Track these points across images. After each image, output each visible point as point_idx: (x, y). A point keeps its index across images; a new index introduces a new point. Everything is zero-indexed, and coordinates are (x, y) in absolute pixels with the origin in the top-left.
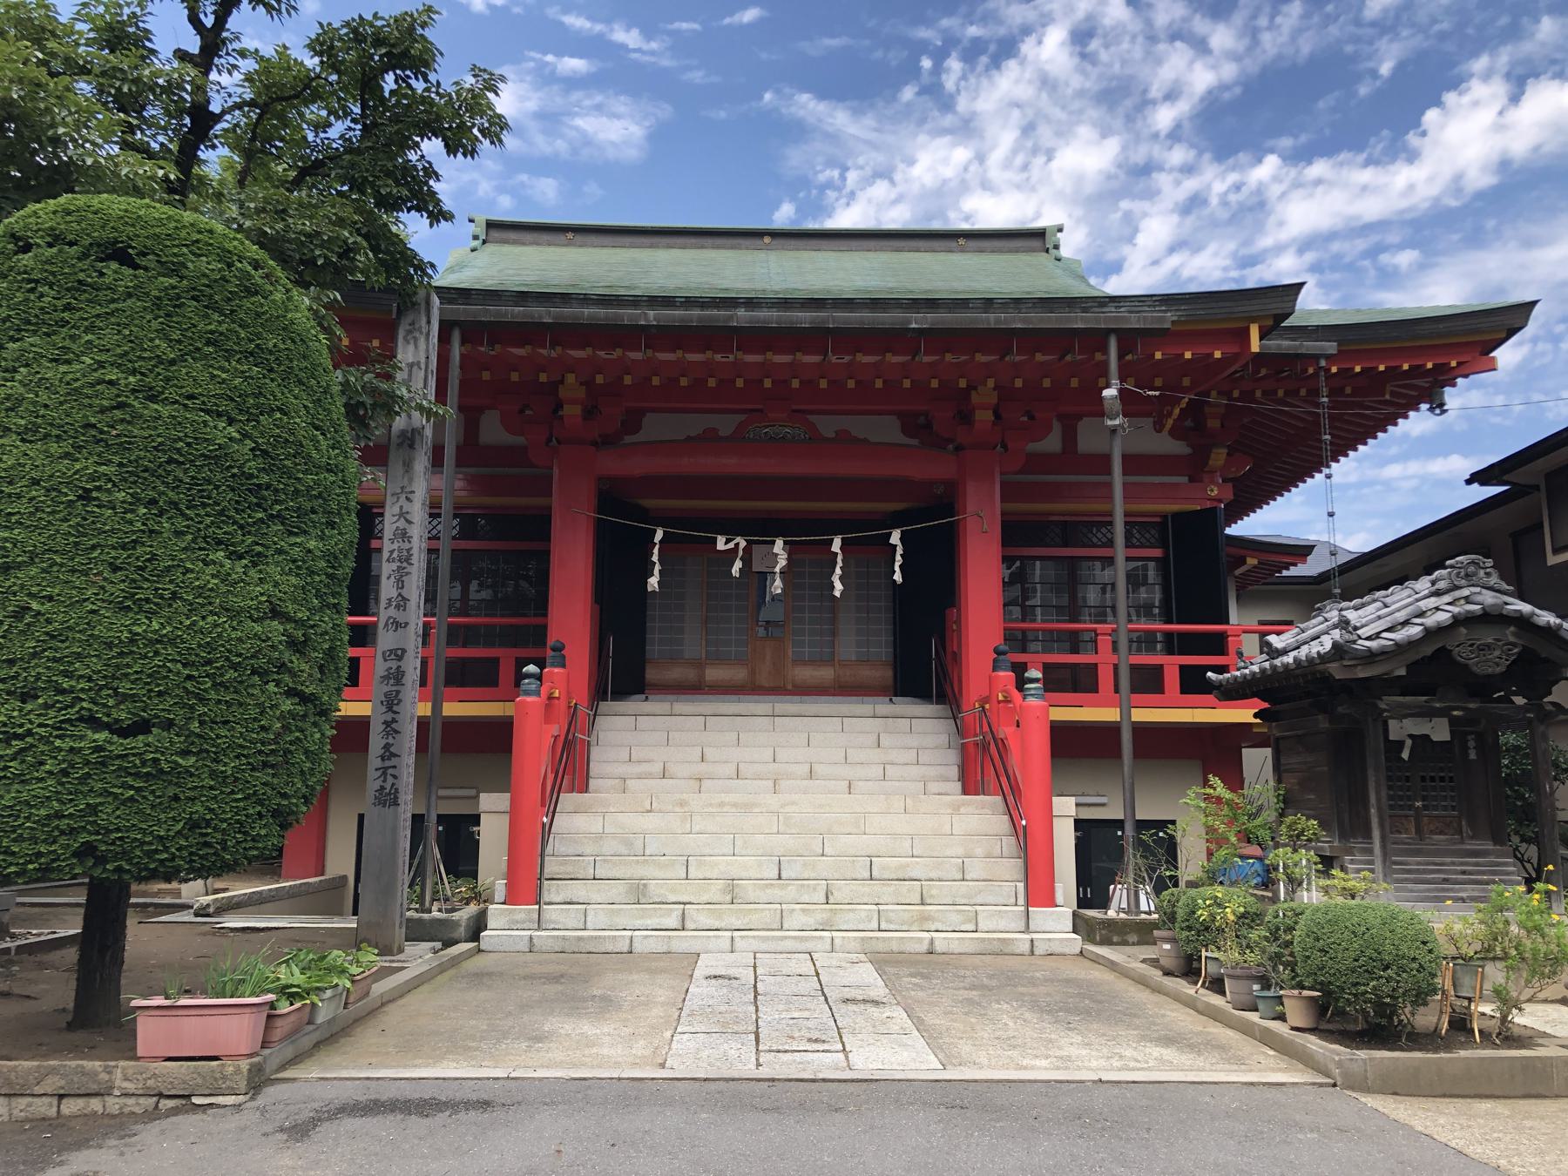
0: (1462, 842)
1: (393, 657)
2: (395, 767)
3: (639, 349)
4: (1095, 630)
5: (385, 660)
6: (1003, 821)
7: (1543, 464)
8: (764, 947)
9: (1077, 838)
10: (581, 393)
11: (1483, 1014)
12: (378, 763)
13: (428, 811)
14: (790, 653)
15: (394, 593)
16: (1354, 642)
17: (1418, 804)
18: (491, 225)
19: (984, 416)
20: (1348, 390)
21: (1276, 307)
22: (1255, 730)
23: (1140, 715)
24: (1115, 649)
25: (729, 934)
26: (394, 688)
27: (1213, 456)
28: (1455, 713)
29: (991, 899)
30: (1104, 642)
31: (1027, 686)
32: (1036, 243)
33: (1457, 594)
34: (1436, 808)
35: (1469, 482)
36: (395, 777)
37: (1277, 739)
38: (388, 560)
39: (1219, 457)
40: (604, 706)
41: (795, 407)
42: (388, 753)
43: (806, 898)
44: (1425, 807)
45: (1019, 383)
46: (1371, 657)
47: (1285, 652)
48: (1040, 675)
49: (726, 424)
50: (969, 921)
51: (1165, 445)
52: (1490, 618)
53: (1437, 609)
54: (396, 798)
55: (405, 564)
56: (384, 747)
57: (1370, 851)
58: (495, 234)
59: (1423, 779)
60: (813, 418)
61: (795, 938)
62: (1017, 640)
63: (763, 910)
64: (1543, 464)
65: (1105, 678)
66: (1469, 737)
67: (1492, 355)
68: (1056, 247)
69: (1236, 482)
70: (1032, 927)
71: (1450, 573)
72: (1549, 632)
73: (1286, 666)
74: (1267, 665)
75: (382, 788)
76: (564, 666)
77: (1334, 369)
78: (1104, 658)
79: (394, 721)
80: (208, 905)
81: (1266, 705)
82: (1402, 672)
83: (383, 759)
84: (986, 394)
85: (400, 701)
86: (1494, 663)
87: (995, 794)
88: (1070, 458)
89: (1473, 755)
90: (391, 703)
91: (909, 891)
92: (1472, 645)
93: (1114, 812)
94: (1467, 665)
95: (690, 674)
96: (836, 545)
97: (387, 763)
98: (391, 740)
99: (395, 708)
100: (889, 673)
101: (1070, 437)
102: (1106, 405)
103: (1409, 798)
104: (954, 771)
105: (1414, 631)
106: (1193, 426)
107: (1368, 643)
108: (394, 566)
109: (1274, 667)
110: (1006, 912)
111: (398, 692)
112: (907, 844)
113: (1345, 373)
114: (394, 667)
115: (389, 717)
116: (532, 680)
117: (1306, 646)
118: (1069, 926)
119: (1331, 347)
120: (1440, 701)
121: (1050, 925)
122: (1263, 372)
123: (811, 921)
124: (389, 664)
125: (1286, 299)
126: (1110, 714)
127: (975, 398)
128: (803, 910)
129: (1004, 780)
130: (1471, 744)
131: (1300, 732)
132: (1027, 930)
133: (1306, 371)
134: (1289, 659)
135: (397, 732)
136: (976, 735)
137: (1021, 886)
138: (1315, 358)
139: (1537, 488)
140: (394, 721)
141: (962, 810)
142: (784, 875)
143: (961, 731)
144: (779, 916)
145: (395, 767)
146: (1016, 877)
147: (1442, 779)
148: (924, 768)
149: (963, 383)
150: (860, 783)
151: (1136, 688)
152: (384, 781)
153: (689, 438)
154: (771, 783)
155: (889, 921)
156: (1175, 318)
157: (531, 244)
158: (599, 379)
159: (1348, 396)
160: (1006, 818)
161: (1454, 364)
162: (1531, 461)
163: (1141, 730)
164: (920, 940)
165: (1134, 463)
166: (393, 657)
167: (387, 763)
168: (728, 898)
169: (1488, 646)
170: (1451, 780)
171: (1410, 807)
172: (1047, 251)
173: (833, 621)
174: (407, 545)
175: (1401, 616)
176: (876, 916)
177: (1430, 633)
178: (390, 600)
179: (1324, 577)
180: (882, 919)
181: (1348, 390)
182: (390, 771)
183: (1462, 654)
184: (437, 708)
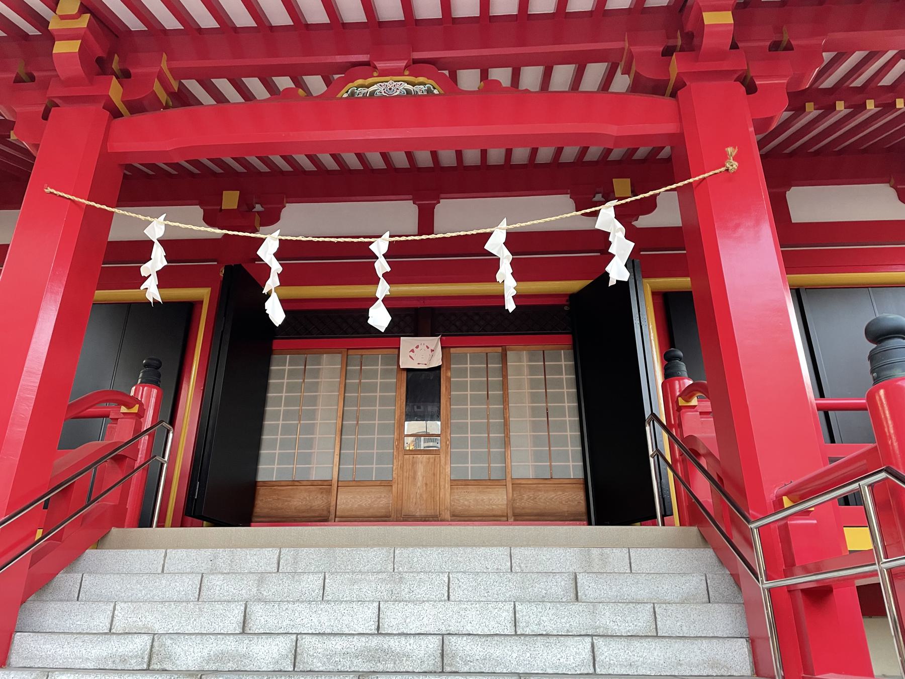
41: (417, 55)
100: (581, 495)
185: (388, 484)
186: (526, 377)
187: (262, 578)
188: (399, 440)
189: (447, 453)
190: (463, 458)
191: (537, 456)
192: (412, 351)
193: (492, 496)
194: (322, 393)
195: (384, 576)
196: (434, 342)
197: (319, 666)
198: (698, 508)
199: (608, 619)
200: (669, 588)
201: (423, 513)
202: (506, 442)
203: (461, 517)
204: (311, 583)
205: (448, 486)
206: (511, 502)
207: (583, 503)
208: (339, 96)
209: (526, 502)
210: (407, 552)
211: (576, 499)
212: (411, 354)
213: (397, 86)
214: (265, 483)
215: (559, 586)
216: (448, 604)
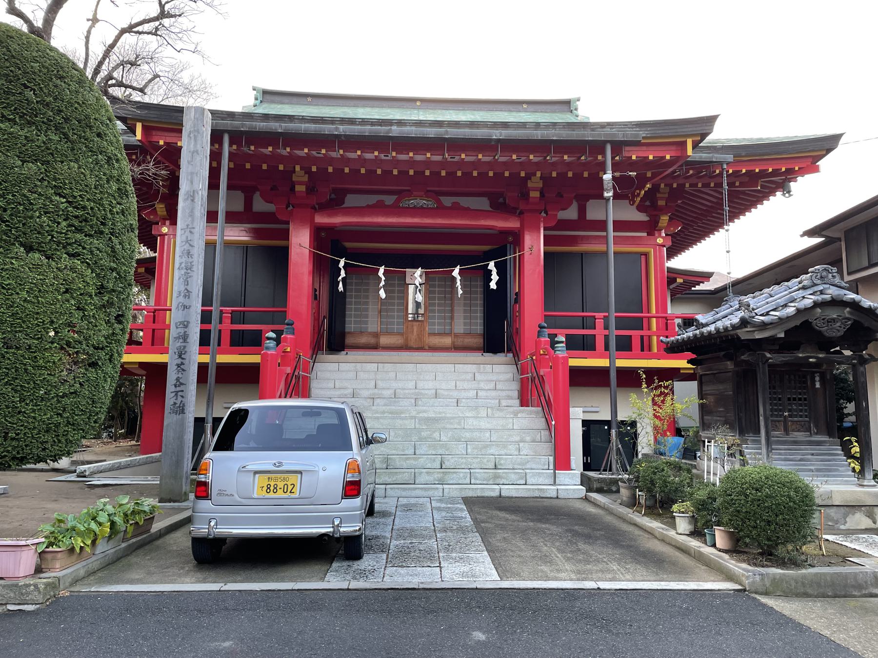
0: (811, 435)
1: (181, 326)
2: (182, 391)
3: (335, 151)
4: (594, 317)
5: (177, 328)
6: (541, 423)
7: (842, 225)
8: (404, 494)
9: (584, 431)
10: (306, 178)
11: (827, 540)
12: (173, 389)
13: (207, 415)
14: (427, 329)
15: (182, 288)
16: (753, 317)
17: (786, 414)
18: (265, 92)
19: (535, 194)
20: (737, 184)
21: (700, 129)
22: (681, 372)
23: (621, 363)
24: (606, 327)
25: (383, 486)
26: (182, 344)
27: (660, 221)
28: (811, 360)
29: (534, 466)
30: (600, 323)
31: (556, 345)
32: (565, 107)
33: (816, 289)
34: (796, 416)
35: (802, 236)
36: (182, 397)
37: (701, 376)
38: (179, 268)
39: (664, 219)
40: (320, 357)
41: (428, 189)
42: (179, 383)
43: (429, 465)
44: (790, 416)
45: (554, 174)
46: (764, 326)
47: (707, 325)
48: (564, 340)
49: (389, 200)
50: (521, 478)
51: (633, 215)
52: (836, 303)
53: (804, 297)
54: (183, 409)
55: (189, 271)
56: (177, 379)
57: (759, 442)
58: (268, 97)
59: (789, 399)
60: (442, 198)
61: (422, 489)
62: (552, 322)
63: (404, 473)
64: (842, 225)
65: (600, 343)
66: (816, 375)
67: (817, 164)
68: (576, 109)
69: (673, 236)
70: (557, 482)
71: (811, 276)
72: (870, 311)
73: (710, 333)
74: (698, 332)
75: (175, 404)
76: (293, 334)
77: (731, 171)
78: (599, 332)
79: (182, 364)
80: (85, 471)
81: (694, 356)
82: (782, 335)
83: (176, 386)
84: (536, 182)
85: (186, 352)
86: (837, 330)
87: (538, 406)
88: (582, 223)
89: (818, 385)
90: (181, 354)
91: (488, 461)
92: (823, 319)
93: (605, 415)
94: (820, 331)
95: (372, 341)
96: (456, 272)
97: (178, 389)
98: (180, 375)
99: (183, 356)
100: (482, 340)
101: (582, 211)
102: (605, 183)
103: (780, 410)
104: (515, 394)
105: (791, 310)
106: (649, 205)
107: (762, 318)
108: (183, 272)
109: (702, 334)
110: (543, 473)
111: (185, 347)
112: (488, 435)
113: (736, 174)
114: (183, 332)
115: (179, 361)
116: (272, 341)
117: (720, 322)
118: (579, 481)
119: (730, 158)
120: (803, 353)
121: (567, 481)
122: (691, 172)
123: (430, 479)
124: (179, 330)
125: (707, 124)
126: (604, 363)
127: (530, 184)
128: (427, 473)
129: (542, 398)
130: (817, 379)
131: (715, 372)
132: (555, 484)
133: (715, 172)
134: (712, 328)
135: (183, 370)
136: (528, 374)
137: (551, 459)
138: (720, 163)
139: (839, 239)
140: (182, 364)
141: (519, 415)
142: (417, 453)
143: (522, 371)
144: (413, 476)
145: (182, 391)
146: (550, 453)
147: (800, 399)
148: (499, 392)
149: (523, 174)
150: (463, 400)
151: (619, 348)
152: (176, 399)
153: (368, 206)
154: (413, 401)
155: (476, 479)
156: (644, 135)
157: (287, 103)
158: (314, 169)
159: (737, 187)
160: (544, 419)
161: (797, 168)
162: (861, 213)
163: (621, 371)
164: (493, 490)
165: (619, 225)
166: (181, 326)
167: (178, 389)
168: (385, 466)
169: (834, 320)
170: (805, 399)
171: (781, 416)
172: (571, 112)
173: (452, 311)
174: (190, 260)
175: (781, 302)
176: (469, 476)
177: (799, 311)
178: (180, 292)
179: (724, 289)
180: (472, 477)
181: (737, 184)
182: (180, 394)
183: (818, 325)
184: (213, 358)
190: (434, 324)
191: (465, 324)
193: (445, 340)
197: (401, 396)
198: (107, 595)
199: (482, 385)
200: (502, 377)
201: (417, 346)
202: (452, 318)
203: (434, 349)
204: (392, 375)
205: (427, 336)
206: (453, 343)
207: (482, 343)
209: (459, 342)
211: (479, 341)
214: (349, 333)
215: (471, 376)
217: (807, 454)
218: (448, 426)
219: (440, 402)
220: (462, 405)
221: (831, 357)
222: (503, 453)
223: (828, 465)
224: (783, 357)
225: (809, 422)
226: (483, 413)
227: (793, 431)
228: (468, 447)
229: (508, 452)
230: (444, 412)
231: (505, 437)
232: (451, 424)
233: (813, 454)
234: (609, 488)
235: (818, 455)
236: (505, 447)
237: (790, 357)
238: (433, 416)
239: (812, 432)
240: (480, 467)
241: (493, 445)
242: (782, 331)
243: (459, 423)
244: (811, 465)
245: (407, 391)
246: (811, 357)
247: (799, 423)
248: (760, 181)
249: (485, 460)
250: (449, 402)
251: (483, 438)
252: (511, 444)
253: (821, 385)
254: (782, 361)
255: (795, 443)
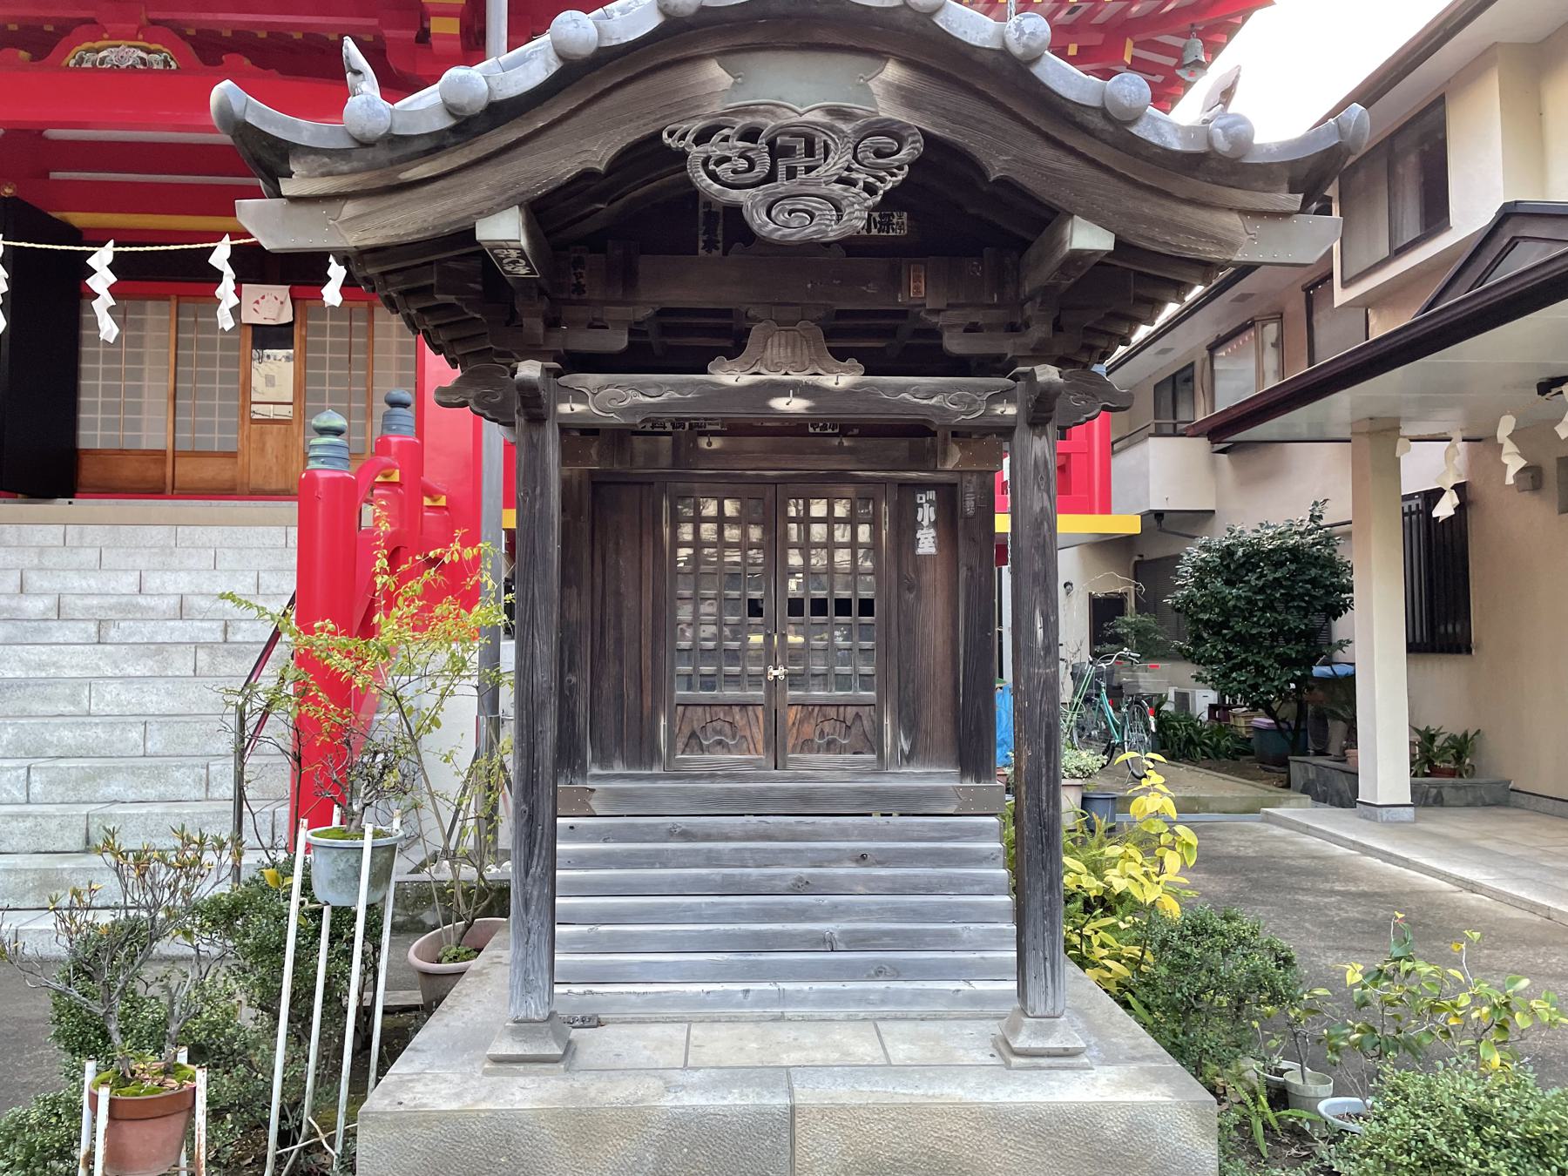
28: (780, 404)
44: (793, 680)
66: (922, 498)
91: (62, 827)
112: (135, 735)
130: (927, 514)
154: (92, 627)
185: (232, 455)
186: (395, 339)
187: (42, 550)
188: (243, 407)
189: (300, 423)
192: (257, 302)
194: (149, 350)
195: (156, 550)
196: (282, 291)
197: (78, 615)
208: (65, 63)
210: (187, 530)
212: (256, 306)
213: (123, 54)
214: (87, 451)
216: (216, 573)
217: (837, 858)
218: (37, 707)
219: (173, 630)
220: (239, 638)
221: (883, 388)
222: (151, 793)
223: (918, 914)
224: (641, 389)
225: (877, 707)
226: (182, 664)
227: (806, 745)
228: (33, 778)
229: (171, 791)
230: (54, 664)
231: (195, 740)
232: (47, 699)
233: (862, 858)
234: (413, 917)
235: (885, 859)
236: (158, 778)
237: (674, 386)
238: (18, 673)
239: (887, 750)
240: (33, 847)
241: (119, 770)
242: (505, 205)
243: (74, 699)
244: (833, 913)
245: (95, 601)
246: (781, 389)
247: (832, 712)
248: (1129, 43)
249: (53, 825)
250: (203, 630)
251: (121, 746)
252: (178, 767)
253: (939, 541)
254: (634, 409)
255: (806, 804)
